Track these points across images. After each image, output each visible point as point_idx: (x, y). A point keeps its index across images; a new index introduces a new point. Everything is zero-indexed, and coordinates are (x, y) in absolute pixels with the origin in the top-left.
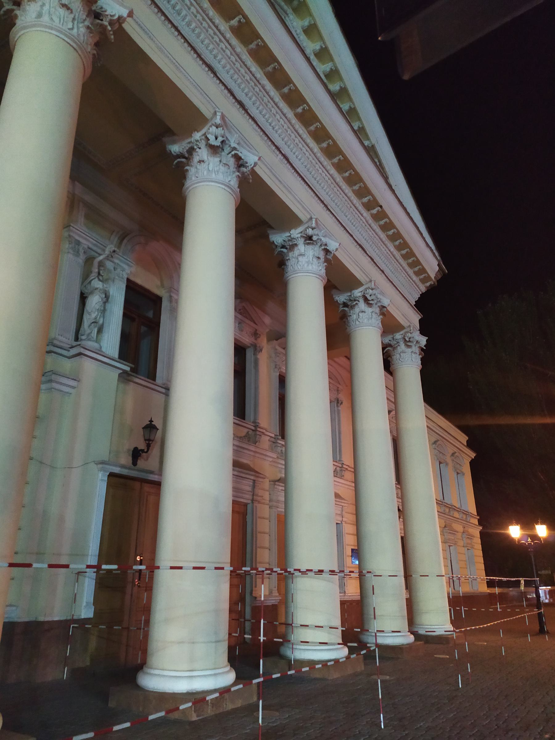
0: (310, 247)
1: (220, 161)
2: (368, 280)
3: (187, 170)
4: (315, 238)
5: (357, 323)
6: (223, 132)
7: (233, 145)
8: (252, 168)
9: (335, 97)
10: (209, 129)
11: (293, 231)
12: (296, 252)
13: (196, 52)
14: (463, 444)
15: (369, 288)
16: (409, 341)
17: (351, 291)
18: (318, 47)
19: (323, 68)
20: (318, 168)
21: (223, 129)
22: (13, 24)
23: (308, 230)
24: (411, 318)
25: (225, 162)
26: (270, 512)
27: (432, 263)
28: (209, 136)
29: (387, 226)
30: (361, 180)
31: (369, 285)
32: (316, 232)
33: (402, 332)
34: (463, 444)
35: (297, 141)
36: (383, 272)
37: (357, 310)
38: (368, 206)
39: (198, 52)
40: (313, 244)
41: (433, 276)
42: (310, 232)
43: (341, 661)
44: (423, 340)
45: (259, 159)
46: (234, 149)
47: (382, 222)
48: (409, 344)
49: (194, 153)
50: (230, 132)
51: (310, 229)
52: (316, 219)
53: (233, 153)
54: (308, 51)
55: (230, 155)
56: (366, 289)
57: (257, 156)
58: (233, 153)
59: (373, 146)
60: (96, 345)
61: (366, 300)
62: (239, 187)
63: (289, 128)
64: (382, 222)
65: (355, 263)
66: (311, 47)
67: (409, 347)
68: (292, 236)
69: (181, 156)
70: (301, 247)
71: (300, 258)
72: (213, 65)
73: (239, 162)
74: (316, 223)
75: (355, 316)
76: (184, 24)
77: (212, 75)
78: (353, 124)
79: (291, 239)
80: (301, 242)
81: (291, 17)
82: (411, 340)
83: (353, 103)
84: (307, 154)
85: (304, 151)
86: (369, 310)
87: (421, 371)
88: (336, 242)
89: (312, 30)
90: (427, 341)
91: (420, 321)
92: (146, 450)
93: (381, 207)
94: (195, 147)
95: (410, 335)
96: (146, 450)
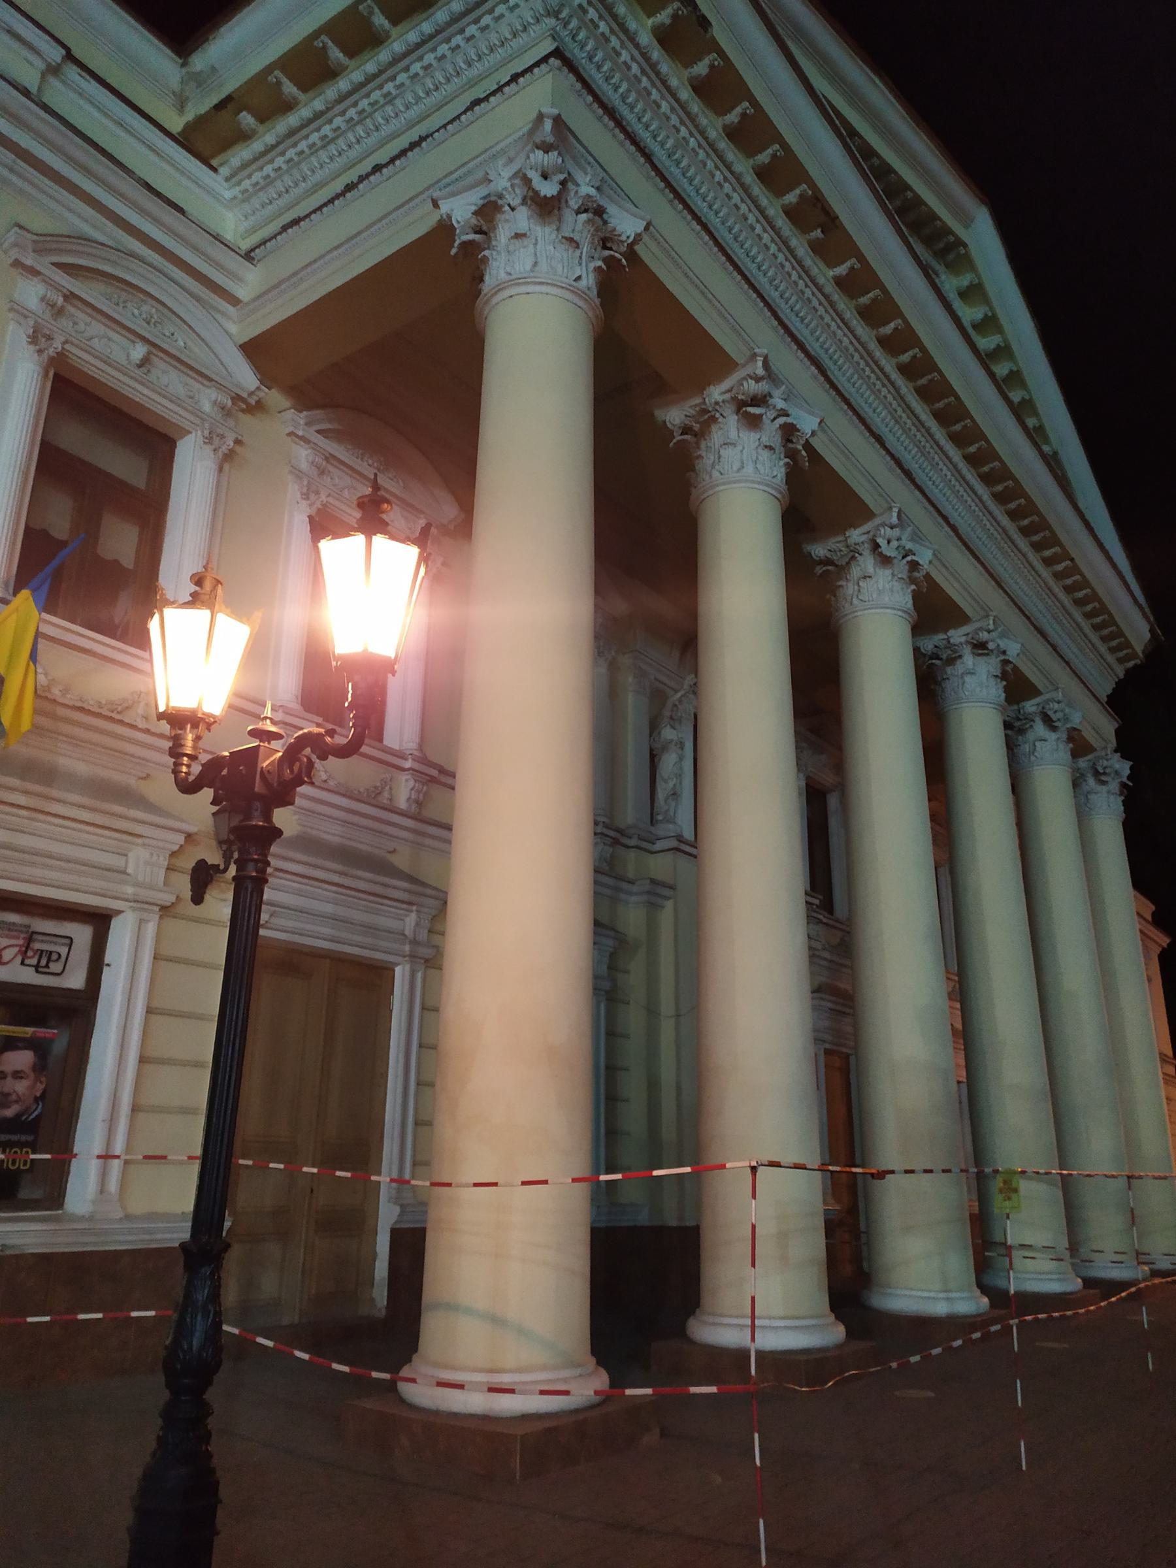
0: (981, 660)
1: (893, 575)
3: (700, 457)
4: (991, 646)
5: (1033, 758)
6: (560, 160)
7: (781, 404)
8: (631, 246)
9: (1003, 385)
10: (528, 157)
11: (951, 633)
12: (959, 668)
13: (664, 179)
14: (1145, 919)
15: (1053, 700)
16: (1104, 774)
17: (1018, 703)
18: (980, 316)
19: (970, 314)
20: (817, 306)
21: (560, 154)
22: (691, 468)
23: (745, 384)
24: (1102, 728)
25: (567, 235)
27: (1138, 629)
28: (879, 540)
29: (782, 172)
30: (875, 282)
33: (1090, 757)
34: (1145, 919)
35: (766, 238)
36: (1068, 663)
37: (1030, 736)
38: (872, 315)
39: (604, 99)
40: (987, 654)
41: (1139, 649)
42: (984, 636)
44: (1124, 767)
45: (647, 228)
46: (784, 413)
47: (905, 358)
48: (1103, 778)
49: (714, 428)
50: (577, 163)
51: (752, 382)
53: (909, 558)
54: (966, 322)
55: (904, 561)
57: (642, 219)
58: (909, 558)
59: (1055, 453)
61: (1097, 774)
62: (599, 295)
63: (726, 179)
64: (905, 358)
65: (856, 462)
66: (970, 314)
67: (1104, 783)
68: (952, 641)
69: (828, 562)
70: (969, 659)
71: (968, 679)
72: (957, 524)
73: (789, 432)
74: (899, 517)
75: (1027, 746)
76: (584, 55)
77: (642, 160)
78: (1011, 395)
79: (949, 645)
80: (967, 651)
81: (943, 277)
82: (1108, 771)
83: (1029, 392)
84: (821, 311)
85: (725, 187)
86: (1053, 736)
88: (812, 413)
89: (974, 292)
90: (1131, 768)
91: (1117, 732)
92: (222, 867)
93: (1072, 560)
94: (718, 415)
95: (1106, 763)
96: (222, 867)
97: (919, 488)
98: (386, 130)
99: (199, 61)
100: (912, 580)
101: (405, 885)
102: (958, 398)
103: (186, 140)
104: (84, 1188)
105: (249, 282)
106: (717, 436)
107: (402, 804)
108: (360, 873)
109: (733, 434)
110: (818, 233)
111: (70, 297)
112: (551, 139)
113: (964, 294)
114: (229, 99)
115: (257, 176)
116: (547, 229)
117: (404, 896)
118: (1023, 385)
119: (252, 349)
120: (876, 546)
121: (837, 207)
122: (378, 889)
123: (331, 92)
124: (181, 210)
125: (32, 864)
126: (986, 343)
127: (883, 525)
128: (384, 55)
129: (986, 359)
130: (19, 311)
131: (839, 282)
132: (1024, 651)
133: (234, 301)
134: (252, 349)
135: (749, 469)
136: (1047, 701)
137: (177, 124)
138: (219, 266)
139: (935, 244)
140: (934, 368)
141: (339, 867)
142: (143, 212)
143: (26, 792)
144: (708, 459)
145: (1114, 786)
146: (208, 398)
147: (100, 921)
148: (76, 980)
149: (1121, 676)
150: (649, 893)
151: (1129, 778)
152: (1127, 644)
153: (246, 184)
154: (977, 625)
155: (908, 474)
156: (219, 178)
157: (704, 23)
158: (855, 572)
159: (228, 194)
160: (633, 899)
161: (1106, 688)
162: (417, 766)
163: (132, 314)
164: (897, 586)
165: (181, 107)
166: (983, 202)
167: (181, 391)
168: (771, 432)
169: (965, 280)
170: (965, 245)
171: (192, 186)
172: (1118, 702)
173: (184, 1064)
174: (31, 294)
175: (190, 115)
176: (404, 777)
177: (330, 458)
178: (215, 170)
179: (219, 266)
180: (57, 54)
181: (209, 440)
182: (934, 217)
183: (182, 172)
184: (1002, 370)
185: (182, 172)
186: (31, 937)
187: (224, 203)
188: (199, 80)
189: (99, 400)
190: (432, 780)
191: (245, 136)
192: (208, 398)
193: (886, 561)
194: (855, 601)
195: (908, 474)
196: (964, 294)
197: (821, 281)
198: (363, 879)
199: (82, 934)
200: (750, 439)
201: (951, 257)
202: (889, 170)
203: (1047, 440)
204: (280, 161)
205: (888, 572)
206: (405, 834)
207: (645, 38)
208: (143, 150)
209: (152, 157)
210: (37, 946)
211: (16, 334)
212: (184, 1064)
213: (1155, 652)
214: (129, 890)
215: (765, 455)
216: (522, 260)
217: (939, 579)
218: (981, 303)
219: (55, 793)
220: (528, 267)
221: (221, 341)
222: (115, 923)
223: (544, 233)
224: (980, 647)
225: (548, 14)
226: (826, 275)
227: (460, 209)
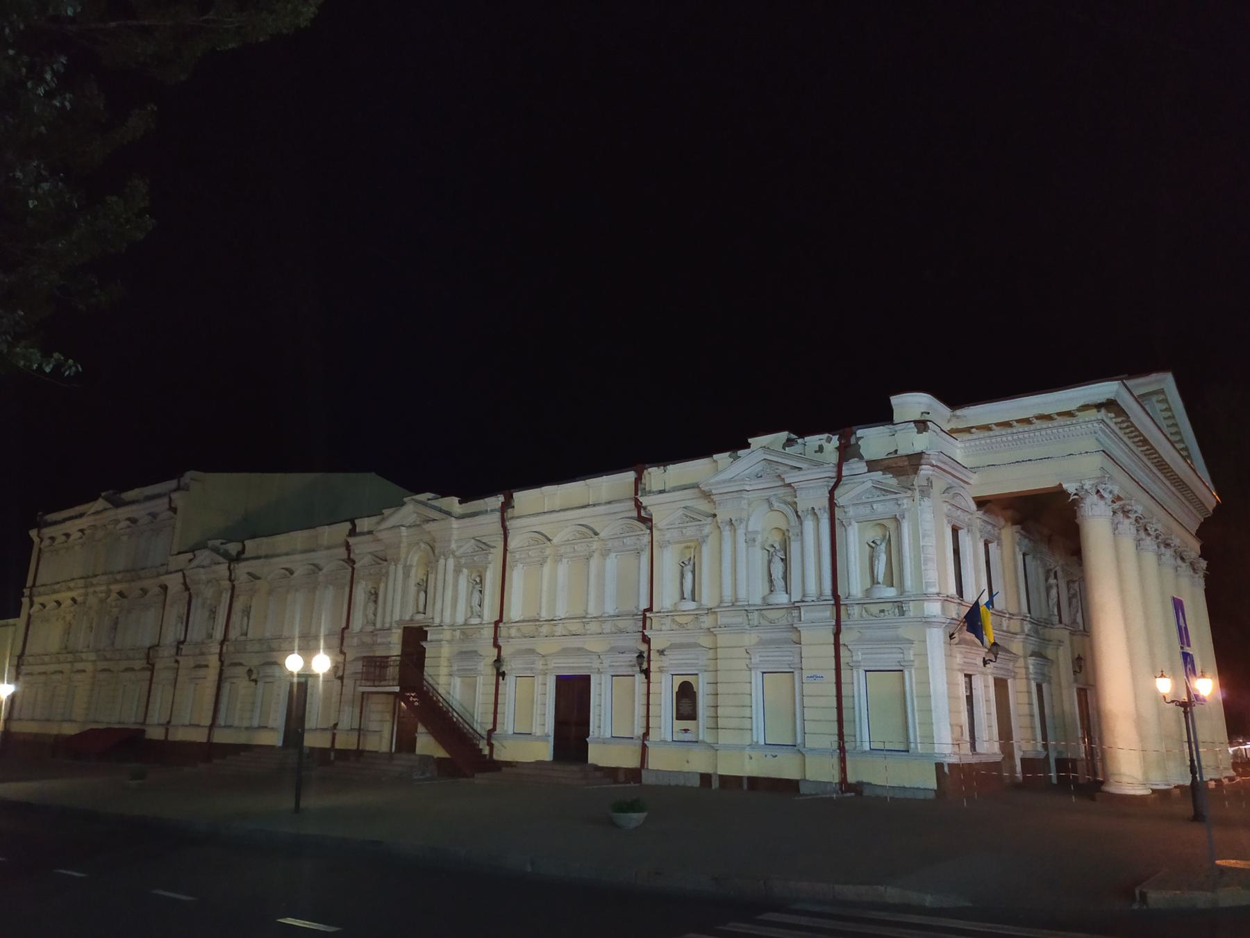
24: (1194, 546)
27: (1211, 499)
105: (974, 479)
145: (1201, 574)
161: (1194, 527)
188: (958, 417)
193: (1149, 535)
200: (1127, 521)
227: (1070, 487)
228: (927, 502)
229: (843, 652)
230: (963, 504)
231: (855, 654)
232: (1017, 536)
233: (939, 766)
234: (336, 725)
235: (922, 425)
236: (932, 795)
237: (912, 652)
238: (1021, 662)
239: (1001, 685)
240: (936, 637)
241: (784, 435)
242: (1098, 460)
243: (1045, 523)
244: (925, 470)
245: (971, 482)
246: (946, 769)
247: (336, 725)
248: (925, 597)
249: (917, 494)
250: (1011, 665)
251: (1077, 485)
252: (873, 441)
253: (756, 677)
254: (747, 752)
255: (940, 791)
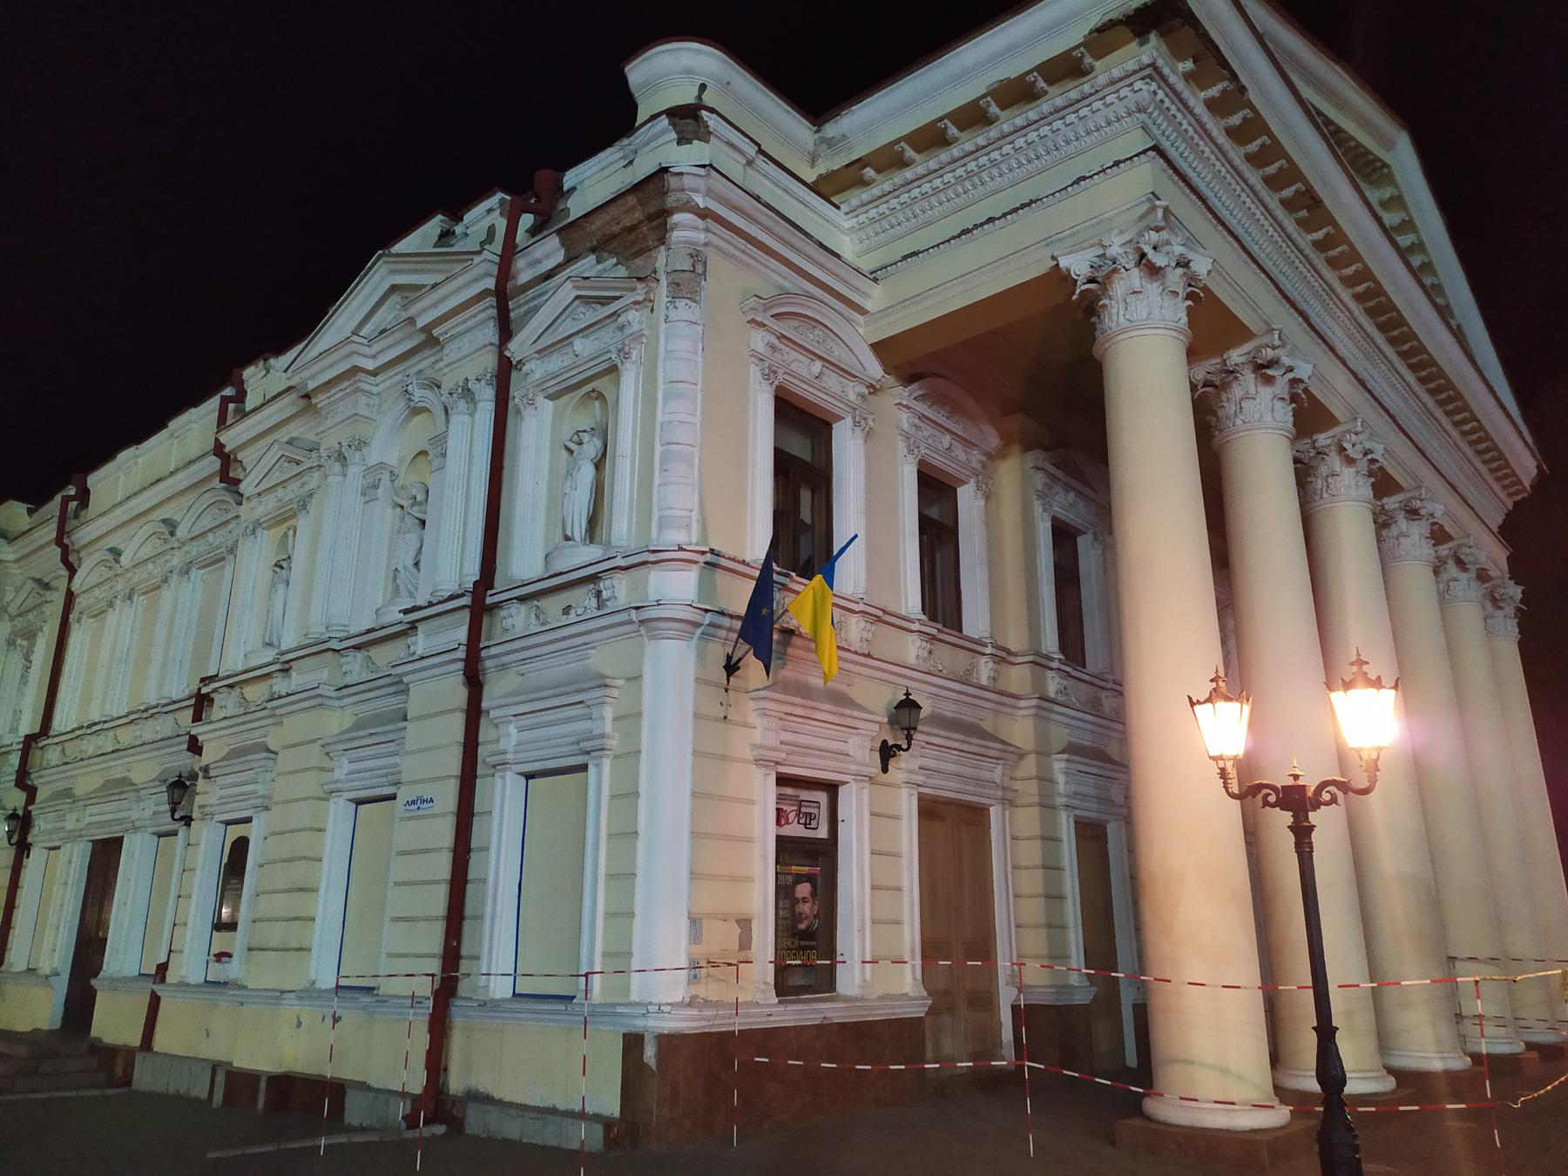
2: (1266, 328)
4: (1423, 512)
15: (1349, 432)
24: (1493, 554)
26: (420, 718)
27: (1526, 465)
28: (1345, 445)
31: (1265, 340)
32: (1280, 353)
41: (1527, 483)
43: (355, 1111)
44: (1516, 592)
46: (1291, 369)
52: (1166, 209)
56: (1258, 349)
60: (593, 552)
67: (1500, 608)
71: (1403, 540)
74: (1165, 217)
80: (1401, 516)
86: (1463, 576)
87: (1520, 643)
89: (1396, 202)
97: (1370, 392)
98: (991, 185)
99: (832, 129)
100: (1371, 474)
101: (998, 746)
102: (1398, 312)
103: (814, 188)
104: (852, 978)
105: (875, 297)
106: (1237, 391)
107: (984, 682)
108: (974, 740)
109: (1252, 390)
110: (1304, 213)
111: (782, 337)
112: (1162, 224)
113: (1383, 204)
114: (859, 160)
115: (873, 213)
116: (1155, 285)
117: (998, 754)
118: (1434, 273)
119: (879, 348)
120: (1342, 449)
121: (1322, 194)
122: (983, 751)
123: (944, 156)
124: (837, 256)
125: (806, 755)
126: (1405, 240)
127: (1349, 432)
128: (993, 132)
129: (1403, 253)
130: (754, 354)
131: (1316, 244)
132: (1447, 513)
133: (863, 311)
134: (879, 348)
135: (1268, 418)
136: (1460, 546)
137: (811, 177)
138: (857, 290)
139: (1363, 167)
140: (1384, 293)
141: (960, 737)
142: (814, 262)
143: (803, 706)
144: (1231, 408)
145: (1509, 610)
146: (853, 391)
147: (832, 788)
148: (823, 833)
149: (1510, 506)
150: (1038, 707)
151: (1522, 601)
152: (1519, 482)
153: (862, 218)
154: (1408, 495)
155: (1362, 383)
156: (841, 213)
157: (1242, 89)
158: (1324, 470)
159: (846, 225)
160: (1021, 712)
161: (1496, 520)
162: (995, 651)
163: (810, 338)
164: (1362, 481)
165: (813, 164)
166: (1403, 127)
167: (837, 389)
168: (1281, 386)
169: (1387, 193)
170: (1388, 166)
171: (821, 221)
172: (1509, 531)
173: (889, 889)
174: (759, 340)
175: (822, 168)
176: (983, 659)
177: (923, 417)
178: (838, 207)
179: (857, 290)
180: (751, 150)
181: (856, 424)
182: (1368, 152)
183: (813, 210)
184: (1416, 261)
185: (813, 210)
186: (800, 803)
187: (843, 229)
188: (830, 143)
189: (791, 404)
190: (1004, 660)
191: (865, 183)
192: (853, 391)
193: (1351, 461)
194: (1325, 495)
195: (1362, 383)
196: (1384, 205)
197: (1303, 245)
198: (975, 744)
199: (822, 797)
200: (1266, 392)
201: (1376, 176)
202: (1339, 130)
203: (1453, 317)
204: (894, 203)
205: (1352, 470)
206: (1089, 727)
207: (1200, 109)
208: (795, 203)
209: (802, 207)
210: (804, 810)
211: (754, 373)
212: (889, 889)
213: (1540, 484)
214: (854, 767)
215: (1279, 404)
216: (1139, 309)
217: (1391, 471)
218: (1398, 212)
219: (818, 705)
220: (1145, 315)
221: (856, 345)
222: (841, 790)
223: (1153, 288)
224: (1413, 513)
225: (1139, 111)
226: (1305, 240)
227: (1078, 265)
228: (684, 310)
229: (485, 733)
230: (847, 360)
231: (505, 737)
232: (1039, 480)
233: (633, 1043)
234: (162, 969)
235: (687, 119)
236: (586, 1136)
237: (609, 712)
238: (1029, 766)
239: (953, 827)
240: (672, 672)
241: (434, 225)
242: (1146, 173)
243: (1028, 378)
244: (685, 230)
245: (868, 305)
246: (650, 1053)
247: (162, 969)
248: (648, 559)
249: (662, 292)
250: (997, 774)
251: (1090, 255)
252: (594, 182)
253: (338, 814)
254: (290, 1008)
255: (623, 1133)
